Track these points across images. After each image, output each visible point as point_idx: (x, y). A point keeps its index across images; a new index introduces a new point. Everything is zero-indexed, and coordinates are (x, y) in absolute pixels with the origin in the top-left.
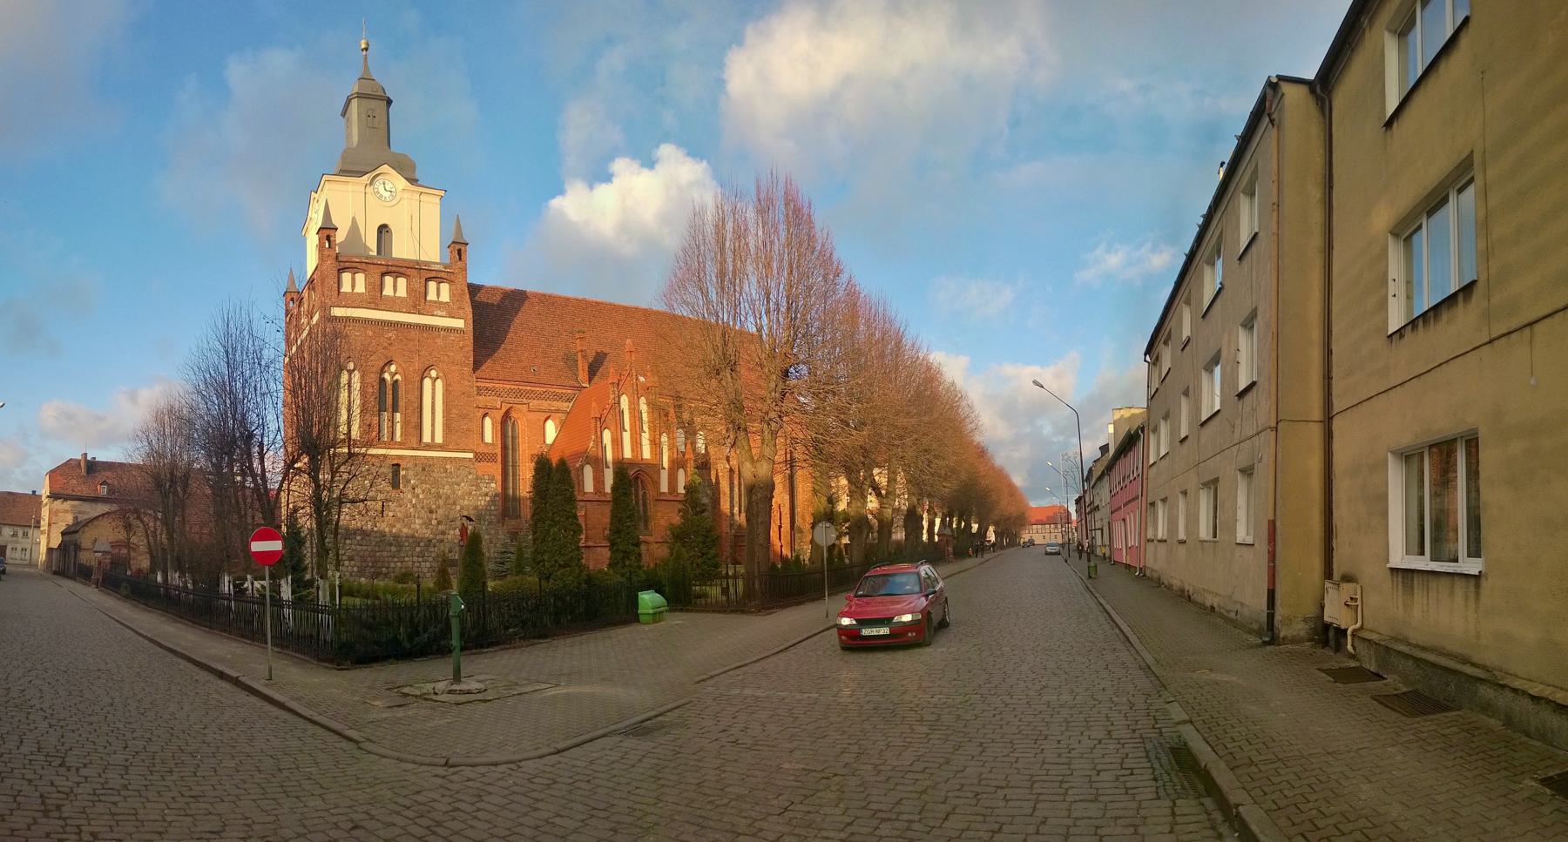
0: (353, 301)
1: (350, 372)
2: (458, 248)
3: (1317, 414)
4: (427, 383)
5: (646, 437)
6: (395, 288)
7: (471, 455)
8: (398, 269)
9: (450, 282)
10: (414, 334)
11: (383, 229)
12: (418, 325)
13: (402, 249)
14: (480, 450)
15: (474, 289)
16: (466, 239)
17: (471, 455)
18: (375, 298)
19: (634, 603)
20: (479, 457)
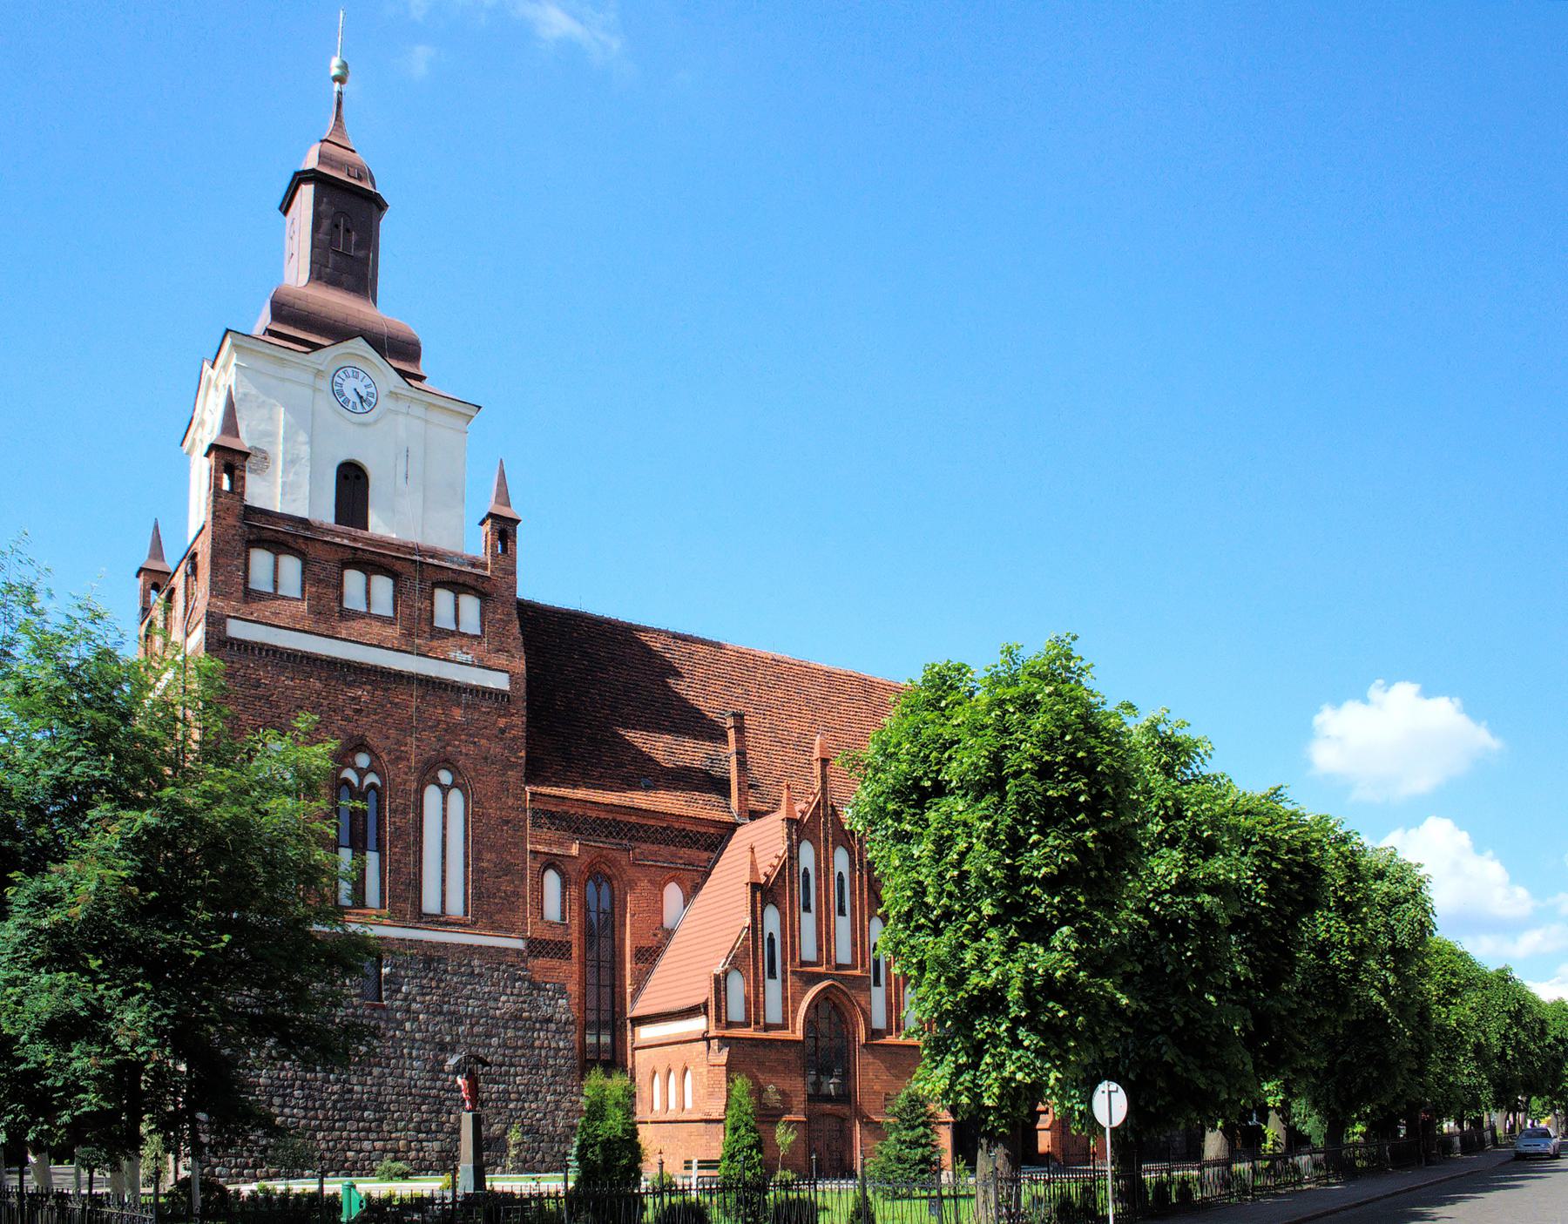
4: (432, 795)
17: (519, 944)
18: (419, 630)
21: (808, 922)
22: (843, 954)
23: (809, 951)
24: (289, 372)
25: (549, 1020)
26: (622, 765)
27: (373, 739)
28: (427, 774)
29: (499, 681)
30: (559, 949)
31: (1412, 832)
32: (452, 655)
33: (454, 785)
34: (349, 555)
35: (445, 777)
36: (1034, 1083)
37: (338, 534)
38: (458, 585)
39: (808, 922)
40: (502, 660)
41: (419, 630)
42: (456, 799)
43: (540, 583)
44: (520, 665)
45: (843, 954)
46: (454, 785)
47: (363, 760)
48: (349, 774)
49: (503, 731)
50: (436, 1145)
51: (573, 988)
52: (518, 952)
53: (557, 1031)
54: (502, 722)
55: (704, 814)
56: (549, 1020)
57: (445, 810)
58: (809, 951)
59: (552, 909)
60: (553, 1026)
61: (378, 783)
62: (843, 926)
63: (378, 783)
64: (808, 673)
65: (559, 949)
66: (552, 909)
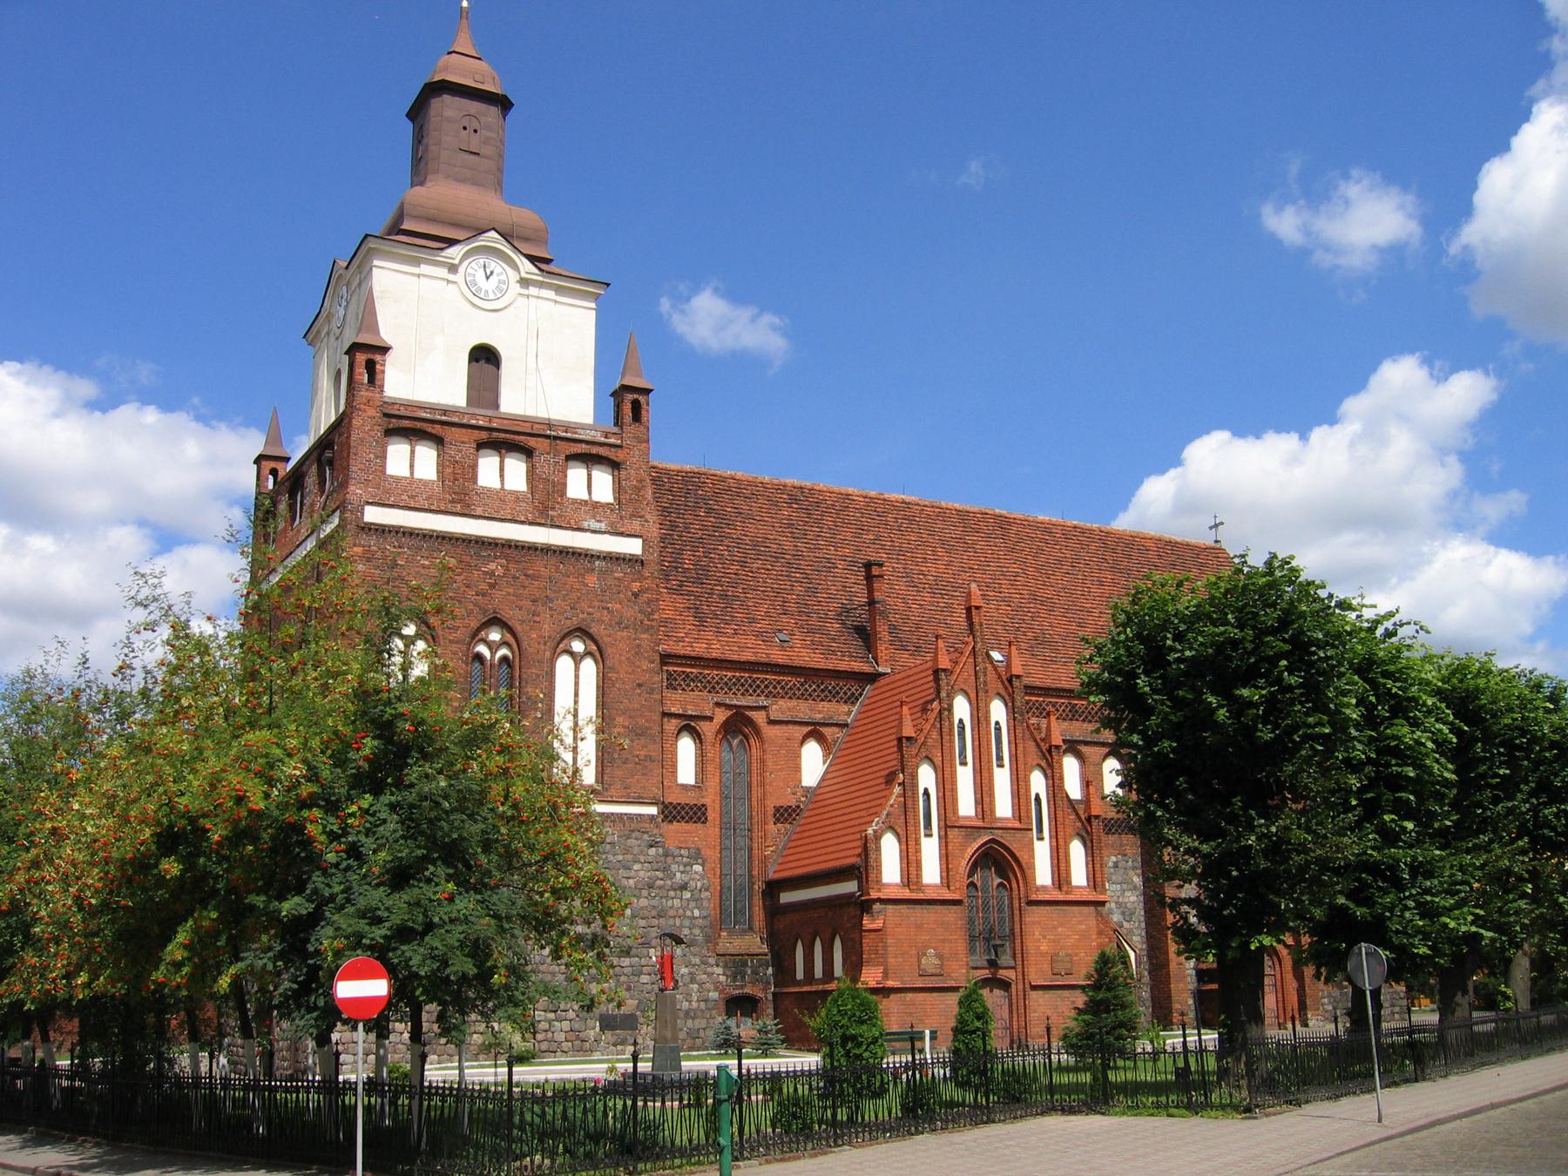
0: (407, 495)
1: (409, 641)
2: (627, 402)
3: (890, 983)
4: (564, 665)
5: (1002, 779)
6: (502, 474)
7: (653, 810)
8: (509, 439)
9: (614, 465)
10: (541, 566)
11: (484, 357)
12: (411, 533)
13: (518, 398)
14: (672, 798)
15: (660, 478)
16: (387, 334)
17: (653, 810)
18: (457, 492)
19: (1210, 1026)
20: (671, 812)
21: (965, 778)
22: (1003, 807)
23: (966, 806)
24: (425, 269)
25: (684, 887)
26: (754, 620)
27: (508, 614)
28: (558, 646)
29: (633, 547)
30: (696, 814)
31: (1318, 434)
32: (585, 524)
33: (588, 653)
34: (484, 435)
35: (578, 646)
36: (1538, 783)
37: (474, 415)
38: (590, 459)
39: (965, 778)
40: (636, 525)
41: (546, 502)
42: (589, 668)
43: (672, 446)
44: (654, 531)
45: (1003, 807)
46: (588, 653)
47: (495, 636)
48: (482, 649)
49: (636, 595)
50: (566, 1025)
51: (712, 854)
52: (652, 818)
53: (693, 898)
54: (636, 586)
55: (843, 666)
56: (684, 887)
57: (577, 677)
58: (966, 806)
59: (686, 772)
60: (687, 895)
61: (509, 654)
62: (1002, 779)
63: (509, 654)
64: (942, 513)
65: (696, 814)
66: (686, 772)
